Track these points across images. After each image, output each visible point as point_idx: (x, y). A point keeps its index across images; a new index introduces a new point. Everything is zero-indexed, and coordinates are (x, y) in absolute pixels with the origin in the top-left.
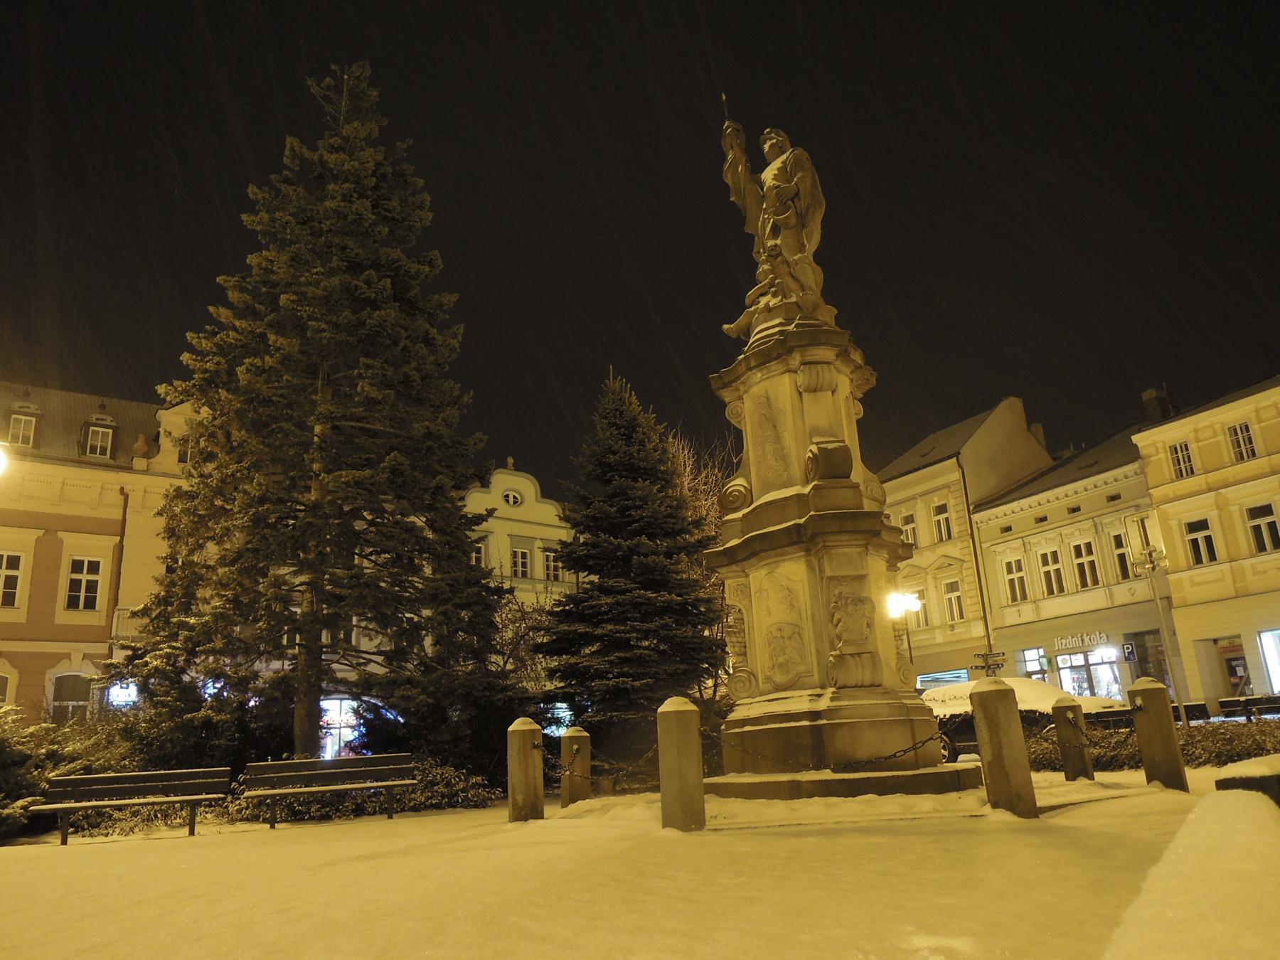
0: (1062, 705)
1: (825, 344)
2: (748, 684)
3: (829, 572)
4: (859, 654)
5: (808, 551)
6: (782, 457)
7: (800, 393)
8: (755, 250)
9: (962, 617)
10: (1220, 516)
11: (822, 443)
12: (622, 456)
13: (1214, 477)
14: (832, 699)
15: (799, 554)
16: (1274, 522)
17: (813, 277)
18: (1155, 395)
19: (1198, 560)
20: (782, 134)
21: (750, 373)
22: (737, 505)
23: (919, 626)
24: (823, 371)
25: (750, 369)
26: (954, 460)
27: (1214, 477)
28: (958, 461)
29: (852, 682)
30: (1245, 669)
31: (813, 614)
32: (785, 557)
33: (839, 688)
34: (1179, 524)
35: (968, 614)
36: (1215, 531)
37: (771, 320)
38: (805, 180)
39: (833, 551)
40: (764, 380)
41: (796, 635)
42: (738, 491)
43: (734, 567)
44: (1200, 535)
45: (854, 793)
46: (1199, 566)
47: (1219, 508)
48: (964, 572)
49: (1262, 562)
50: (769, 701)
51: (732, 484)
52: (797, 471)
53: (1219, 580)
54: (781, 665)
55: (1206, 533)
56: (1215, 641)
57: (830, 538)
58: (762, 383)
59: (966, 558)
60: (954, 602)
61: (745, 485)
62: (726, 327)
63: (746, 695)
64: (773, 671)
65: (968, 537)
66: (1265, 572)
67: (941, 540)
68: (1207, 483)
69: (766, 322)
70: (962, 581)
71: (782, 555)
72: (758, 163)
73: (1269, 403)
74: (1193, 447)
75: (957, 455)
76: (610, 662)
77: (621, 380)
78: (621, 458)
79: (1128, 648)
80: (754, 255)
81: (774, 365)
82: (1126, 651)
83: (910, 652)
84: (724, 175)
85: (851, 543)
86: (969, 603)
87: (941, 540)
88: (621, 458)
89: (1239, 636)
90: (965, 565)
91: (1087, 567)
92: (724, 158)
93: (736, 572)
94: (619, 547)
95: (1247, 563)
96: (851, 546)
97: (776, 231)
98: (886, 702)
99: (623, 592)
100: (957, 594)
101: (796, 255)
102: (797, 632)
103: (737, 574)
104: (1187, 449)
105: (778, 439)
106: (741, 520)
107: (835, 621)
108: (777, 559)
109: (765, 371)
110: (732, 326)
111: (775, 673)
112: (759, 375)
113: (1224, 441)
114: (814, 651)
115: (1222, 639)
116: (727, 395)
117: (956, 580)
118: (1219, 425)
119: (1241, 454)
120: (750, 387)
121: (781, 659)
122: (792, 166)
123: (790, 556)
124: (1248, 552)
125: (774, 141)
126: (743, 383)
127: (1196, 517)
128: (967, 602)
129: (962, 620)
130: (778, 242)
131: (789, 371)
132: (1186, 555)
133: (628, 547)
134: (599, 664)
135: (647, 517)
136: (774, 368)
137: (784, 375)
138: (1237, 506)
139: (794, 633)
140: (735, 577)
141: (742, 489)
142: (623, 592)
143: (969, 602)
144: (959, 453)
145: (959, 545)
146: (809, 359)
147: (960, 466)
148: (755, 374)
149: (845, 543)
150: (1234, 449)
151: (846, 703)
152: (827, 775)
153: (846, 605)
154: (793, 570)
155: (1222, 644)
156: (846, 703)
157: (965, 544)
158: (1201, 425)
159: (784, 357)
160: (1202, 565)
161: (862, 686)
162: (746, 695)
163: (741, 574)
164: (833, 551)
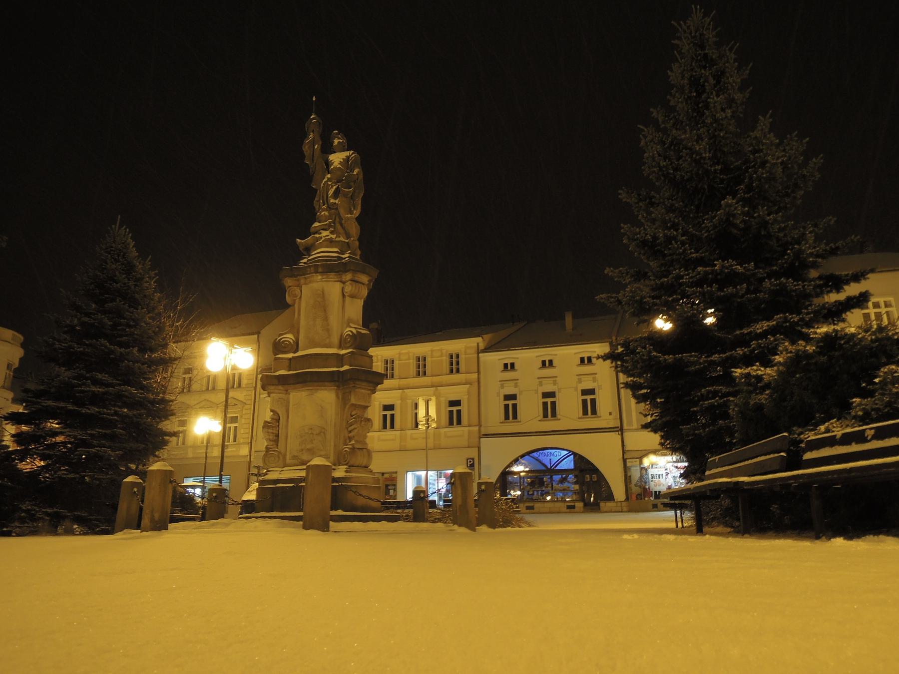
0: (418, 489)
1: (367, 274)
2: (277, 459)
3: (353, 401)
4: (362, 449)
5: (338, 387)
6: (327, 329)
7: (344, 296)
8: (316, 199)
9: (235, 440)
10: (401, 404)
11: (358, 328)
12: (122, 285)
13: (404, 382)
14: (346, 472)
15: (333, 388)
16: (393, 414)
17: (354, 229)
18: (376, 327)
19: (385, 427)
20: (345, 138)
21: (314, 274)
22: (286, 350)
23: (177, 445)
24: (362, 290)
25: (316, 272)
26: (256, 336)
27: (404, 382)
28: (258, 337)
29: (357, 464)
30: (395, 490)
31: (335, 424)
32: (322, 388)
33: (350, 466)
34: (380, 404)
35: (240, 439)
36: (397, 412)
37: (331, 247)
38: (361, 177)
39: (357, 390)
40: (322, 281)
41: (322, 434)
42: (289, 341)
43: (280, 387)
44: (388, 413)
45: (378, 521)
46: (392, 430)
47: (402, 399)
48: (244, 410)
49: (415, 434)
50: (301, 470)
51: (285, 336)
52: (335, 340)
53: (393, 440)
54: (309, 450)
55: (392, 412)
56: (383, 474)
57: (357, 382)
58: (320, 283)
59: (249, 402)
60: (455, 413)
61: (293, 338)
62: (299, 240)
63: (274, 465)
64: (301, 453)
65: (253, 388)
66: (417, 439)
67: (208, 389)
68: (399, 385)
69: (328, 247)
70: (241, 417)
71: (321, 386)
72: (328, 149)
73: (438, 348)
74: (396, 363)
75: (258, 333)
76: (92, 435)
77: (125, 229)
78: (121, 286)
79: (470, 462)
80: (314, 202)
81: (332, 275)
82: (469, 463)
83: (206, 459)
84: (303, 145)
85: (367, 387)
86: (242, 432)
87: (208, 389)
88: (121, 286)
89: (396, 473)
90: (247, 407)
91: (455, 413)
92: (305, 136)
93: (280, 390)
94: (112, 352)
95: (409, 432)
96: (365, 389)
97: (336, 194)
98: (372, 476)
99: (112, 385)
100: (236, 425)
101: (348, 214)
102: (322, 432)
103: (280, 391)
104: (393, 363)
105: (326, 319)
106: (290, 359)
107: (350, 429)
108: (318, 388)
109: (324, 277)
110: (303, 241)
111: (302, 454)
112: (320, 277)
113: (413, 363)
114: (332, 444)
115: (386, 473)
116: (288, 282)
117: (236, 415)
118: (412, 354)
119: (419, 372)
120: (310, 282)
121: (309, 446)
122: (352, 162)
123: (326, 388)
124: (378, 428)
125: (341, 141)
126: (305, 278)
127: (454, 398)
128: (241, 431)
129: (234, 443)
130: (337, 201)
131: (341, 281)
132: (412, 421)
133: (121, 353)
134: (81, 435)
135: (137, 335)
136: (331, 276)
137: (337, 283)
138: (411, 400)
139: (321, 432)
140: (279, 393)
141: (291, 341)
142: (112, 385)
143: (242, 431)
144: (260, 333)
145: (245, 393)
146: (356, 279)
147: (258, 341)
148: (317, 276)
149: (364, 387)
150: (384, 364)
151: (354, 475)
152: (340, 512)
153: (361, 421)
154: (327, 396)
155: (386, 476)
156: (354, 475)
157: (250, 393)
158: (403, 352)
159: (341, 273)
160: (386, 430)
161: (360, 467)
162: (274, 465)
163: (284, 392)
164: (357, 390)
